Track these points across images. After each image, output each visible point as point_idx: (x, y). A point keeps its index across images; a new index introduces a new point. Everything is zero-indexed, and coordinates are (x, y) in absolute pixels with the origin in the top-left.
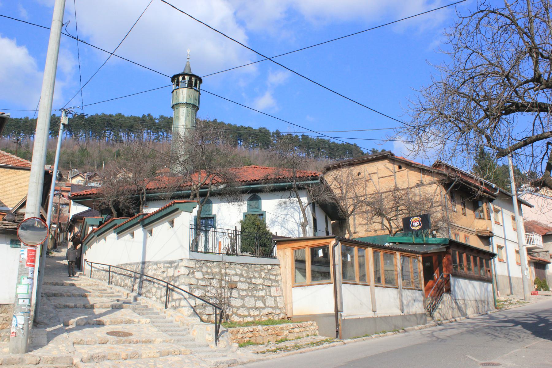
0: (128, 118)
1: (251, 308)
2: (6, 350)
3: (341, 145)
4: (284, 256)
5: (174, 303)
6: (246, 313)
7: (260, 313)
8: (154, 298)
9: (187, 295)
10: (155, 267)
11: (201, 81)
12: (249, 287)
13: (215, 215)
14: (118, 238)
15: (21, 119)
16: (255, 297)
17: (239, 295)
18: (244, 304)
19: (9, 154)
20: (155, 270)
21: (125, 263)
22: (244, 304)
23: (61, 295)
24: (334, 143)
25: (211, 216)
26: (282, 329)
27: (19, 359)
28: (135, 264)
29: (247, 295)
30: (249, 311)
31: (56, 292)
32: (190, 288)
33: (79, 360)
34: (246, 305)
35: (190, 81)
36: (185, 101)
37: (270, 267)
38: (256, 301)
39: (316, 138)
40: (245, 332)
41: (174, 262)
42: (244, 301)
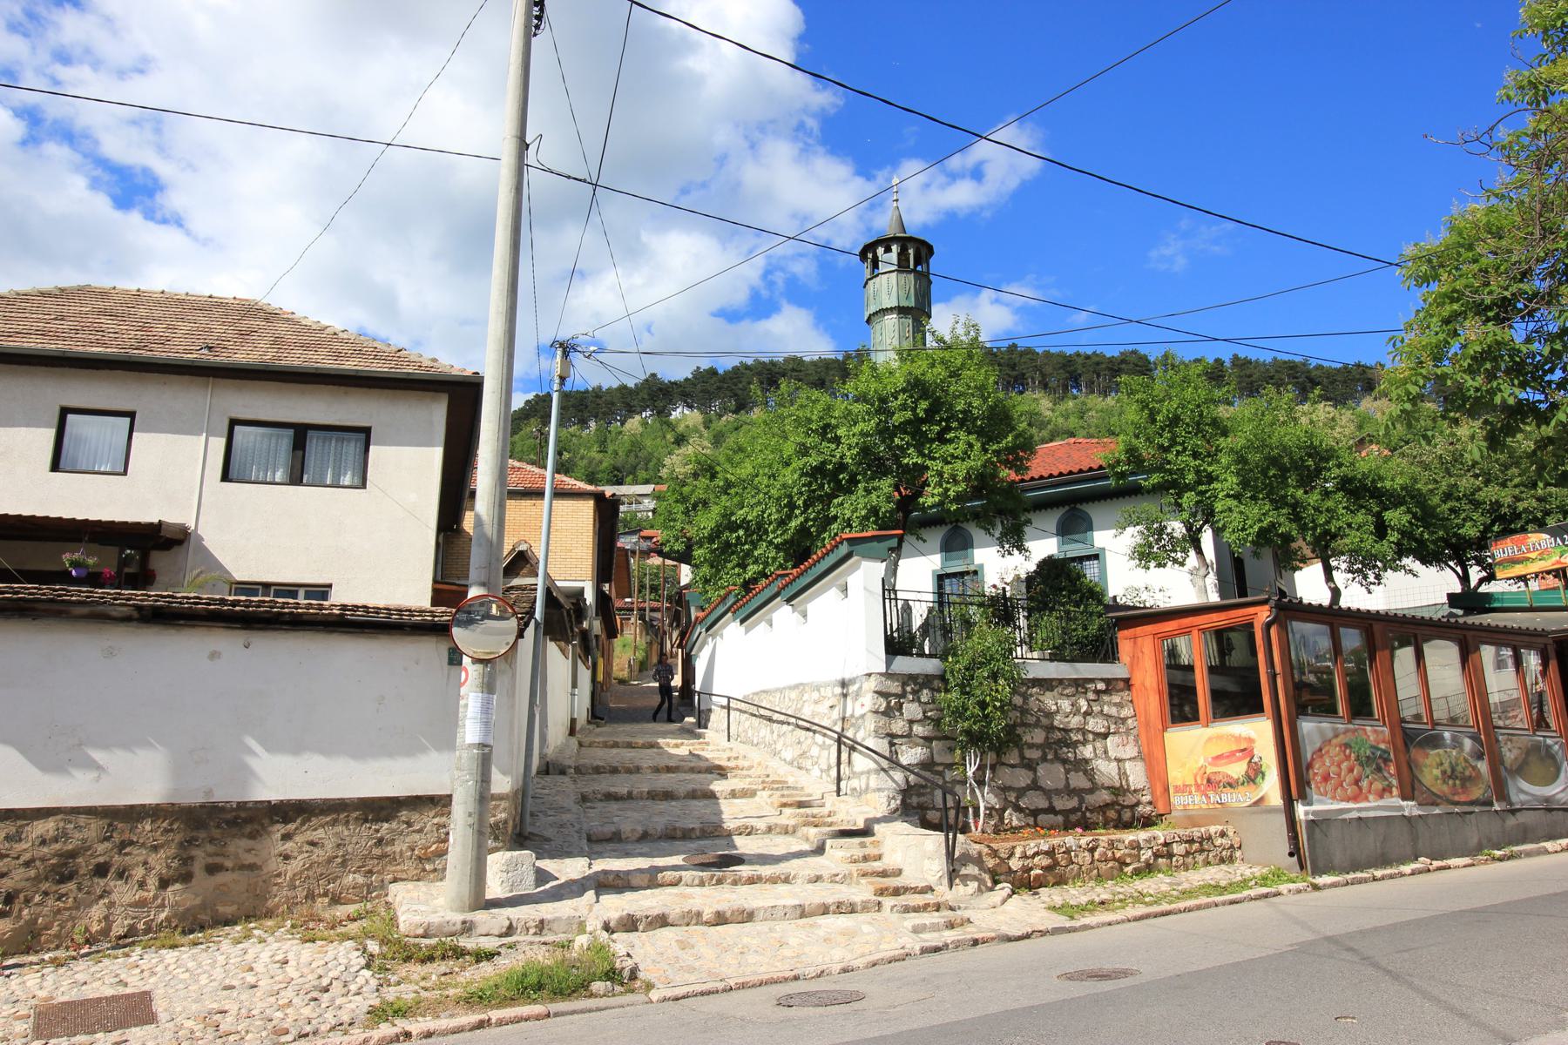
0: (813, 363)
1: (1058, 792)
2: (441, 901)
3: (1338, 370)
4: (1139, 657)
5: (855, 783)
6: (1043, 804)
7: (1080, 804)
8: (816, 772)
9: (885, 764)
10: (815, 695)
11: (930, 250)
12: (1047, 738)
13: (982, 566)
14: (747, 632)
15: (587, 391)
16: (1065, 761)
17: (1022, 757)
18: (1035, 781)
19: (523, 465)
20: (816, 702)
21: (758, 689)
22: (1035, 781)
23: (614, 771)
24: (1319, 367)
25: (972, 568)
26: (1136, 846)
27: (464, 922)
28: (777, 690)
29: (1044, 759)
30: (1049, 799)
31: (601, 764)
32: (892, 744)
33: (600, 925)
34: (1041, 783)
35: (903, 255)
36: (894, 304)
37: (1101, 686)
38: (1067, 772)
39: (1269, 360)
40: (1030, 853)
41: (852, 681)
42: (1035, 771)
